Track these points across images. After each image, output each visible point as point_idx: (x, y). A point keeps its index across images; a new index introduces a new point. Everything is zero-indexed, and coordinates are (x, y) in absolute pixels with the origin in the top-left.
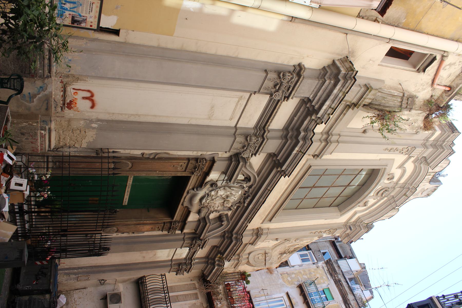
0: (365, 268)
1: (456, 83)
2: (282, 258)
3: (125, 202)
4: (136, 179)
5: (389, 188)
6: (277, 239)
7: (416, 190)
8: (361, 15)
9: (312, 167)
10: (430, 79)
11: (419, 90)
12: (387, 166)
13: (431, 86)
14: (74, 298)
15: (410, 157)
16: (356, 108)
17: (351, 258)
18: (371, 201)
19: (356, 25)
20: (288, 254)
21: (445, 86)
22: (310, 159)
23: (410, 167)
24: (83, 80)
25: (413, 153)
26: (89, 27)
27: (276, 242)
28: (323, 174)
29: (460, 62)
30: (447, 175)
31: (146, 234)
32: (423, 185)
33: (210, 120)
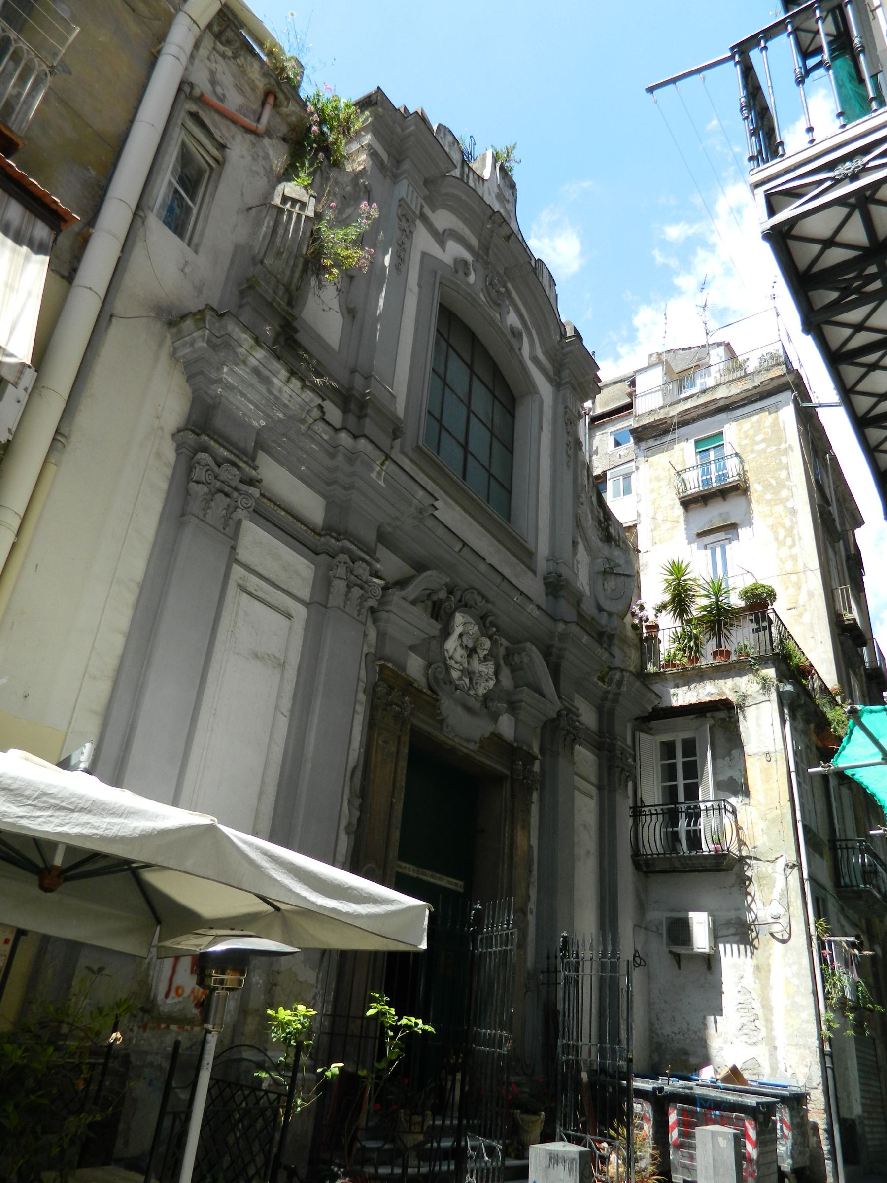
0: (661, 354)
1: (258, 77)
2: (617, 538)
3: (456, 885)
4: (403, 856)
5: (487, 276)
6: (575, 544)
7: (498, 212)
8: (66, 274)
9: (420, 443)
10: (243, 137)
11: (268, 168)
12: (436, 273)
13: (262, 138)
14: (673, 1035)
15: (423, 218)
16: (295, 324)
17: (633, 384)
18: (512, 319)
19: (90, 289)
20: (610, 523)
21: (263, 104)
22: (402, 446)
23: (443, 219)
24: (148, 968)
25: (413, 207)
26: (8, 948)
27: (581, 547)
28: (440, 422)
29: (209, 59)
30: (471, 136)
31: (534, 842)
32: (490, 194)
33: (286, 665)
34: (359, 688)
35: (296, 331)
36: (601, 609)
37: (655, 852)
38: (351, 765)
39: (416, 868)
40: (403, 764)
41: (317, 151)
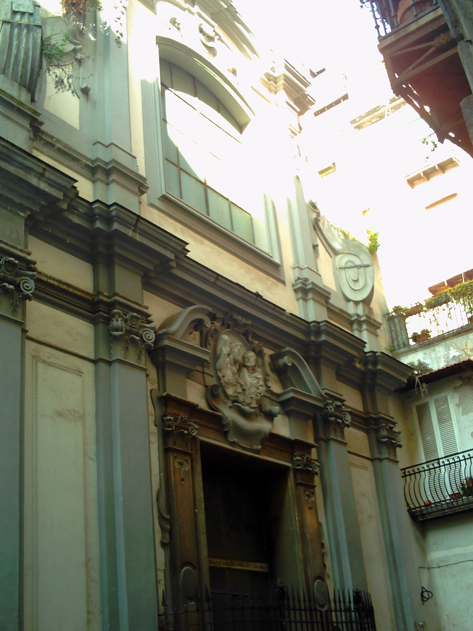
3: (262, 567)
34: (150, 421)
35: (41, 123)
36: (348, 300)
37: (417, 505)
38: (156, 487)
39: (225, 561)
40: (199, 478)
41: (68, 78)
